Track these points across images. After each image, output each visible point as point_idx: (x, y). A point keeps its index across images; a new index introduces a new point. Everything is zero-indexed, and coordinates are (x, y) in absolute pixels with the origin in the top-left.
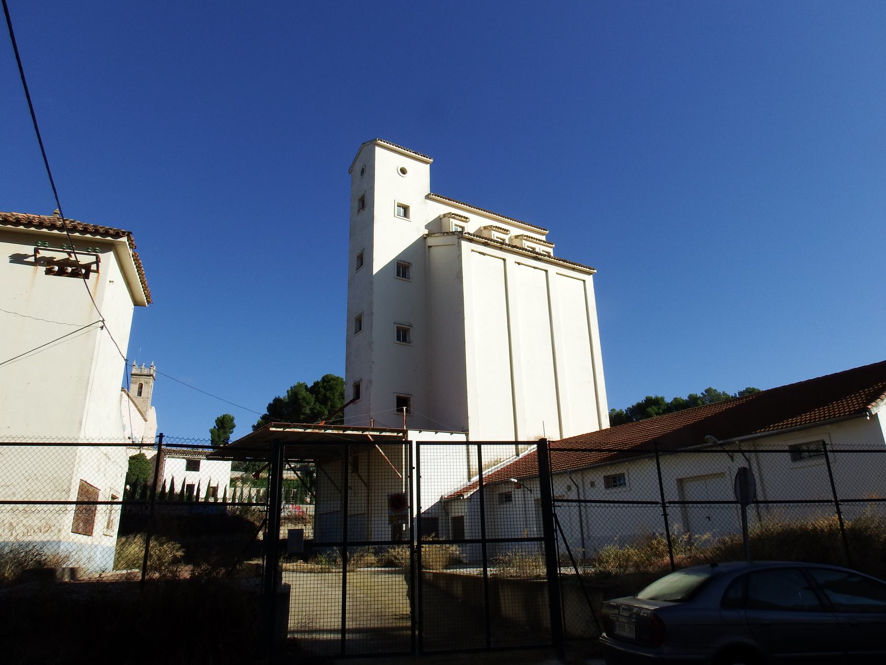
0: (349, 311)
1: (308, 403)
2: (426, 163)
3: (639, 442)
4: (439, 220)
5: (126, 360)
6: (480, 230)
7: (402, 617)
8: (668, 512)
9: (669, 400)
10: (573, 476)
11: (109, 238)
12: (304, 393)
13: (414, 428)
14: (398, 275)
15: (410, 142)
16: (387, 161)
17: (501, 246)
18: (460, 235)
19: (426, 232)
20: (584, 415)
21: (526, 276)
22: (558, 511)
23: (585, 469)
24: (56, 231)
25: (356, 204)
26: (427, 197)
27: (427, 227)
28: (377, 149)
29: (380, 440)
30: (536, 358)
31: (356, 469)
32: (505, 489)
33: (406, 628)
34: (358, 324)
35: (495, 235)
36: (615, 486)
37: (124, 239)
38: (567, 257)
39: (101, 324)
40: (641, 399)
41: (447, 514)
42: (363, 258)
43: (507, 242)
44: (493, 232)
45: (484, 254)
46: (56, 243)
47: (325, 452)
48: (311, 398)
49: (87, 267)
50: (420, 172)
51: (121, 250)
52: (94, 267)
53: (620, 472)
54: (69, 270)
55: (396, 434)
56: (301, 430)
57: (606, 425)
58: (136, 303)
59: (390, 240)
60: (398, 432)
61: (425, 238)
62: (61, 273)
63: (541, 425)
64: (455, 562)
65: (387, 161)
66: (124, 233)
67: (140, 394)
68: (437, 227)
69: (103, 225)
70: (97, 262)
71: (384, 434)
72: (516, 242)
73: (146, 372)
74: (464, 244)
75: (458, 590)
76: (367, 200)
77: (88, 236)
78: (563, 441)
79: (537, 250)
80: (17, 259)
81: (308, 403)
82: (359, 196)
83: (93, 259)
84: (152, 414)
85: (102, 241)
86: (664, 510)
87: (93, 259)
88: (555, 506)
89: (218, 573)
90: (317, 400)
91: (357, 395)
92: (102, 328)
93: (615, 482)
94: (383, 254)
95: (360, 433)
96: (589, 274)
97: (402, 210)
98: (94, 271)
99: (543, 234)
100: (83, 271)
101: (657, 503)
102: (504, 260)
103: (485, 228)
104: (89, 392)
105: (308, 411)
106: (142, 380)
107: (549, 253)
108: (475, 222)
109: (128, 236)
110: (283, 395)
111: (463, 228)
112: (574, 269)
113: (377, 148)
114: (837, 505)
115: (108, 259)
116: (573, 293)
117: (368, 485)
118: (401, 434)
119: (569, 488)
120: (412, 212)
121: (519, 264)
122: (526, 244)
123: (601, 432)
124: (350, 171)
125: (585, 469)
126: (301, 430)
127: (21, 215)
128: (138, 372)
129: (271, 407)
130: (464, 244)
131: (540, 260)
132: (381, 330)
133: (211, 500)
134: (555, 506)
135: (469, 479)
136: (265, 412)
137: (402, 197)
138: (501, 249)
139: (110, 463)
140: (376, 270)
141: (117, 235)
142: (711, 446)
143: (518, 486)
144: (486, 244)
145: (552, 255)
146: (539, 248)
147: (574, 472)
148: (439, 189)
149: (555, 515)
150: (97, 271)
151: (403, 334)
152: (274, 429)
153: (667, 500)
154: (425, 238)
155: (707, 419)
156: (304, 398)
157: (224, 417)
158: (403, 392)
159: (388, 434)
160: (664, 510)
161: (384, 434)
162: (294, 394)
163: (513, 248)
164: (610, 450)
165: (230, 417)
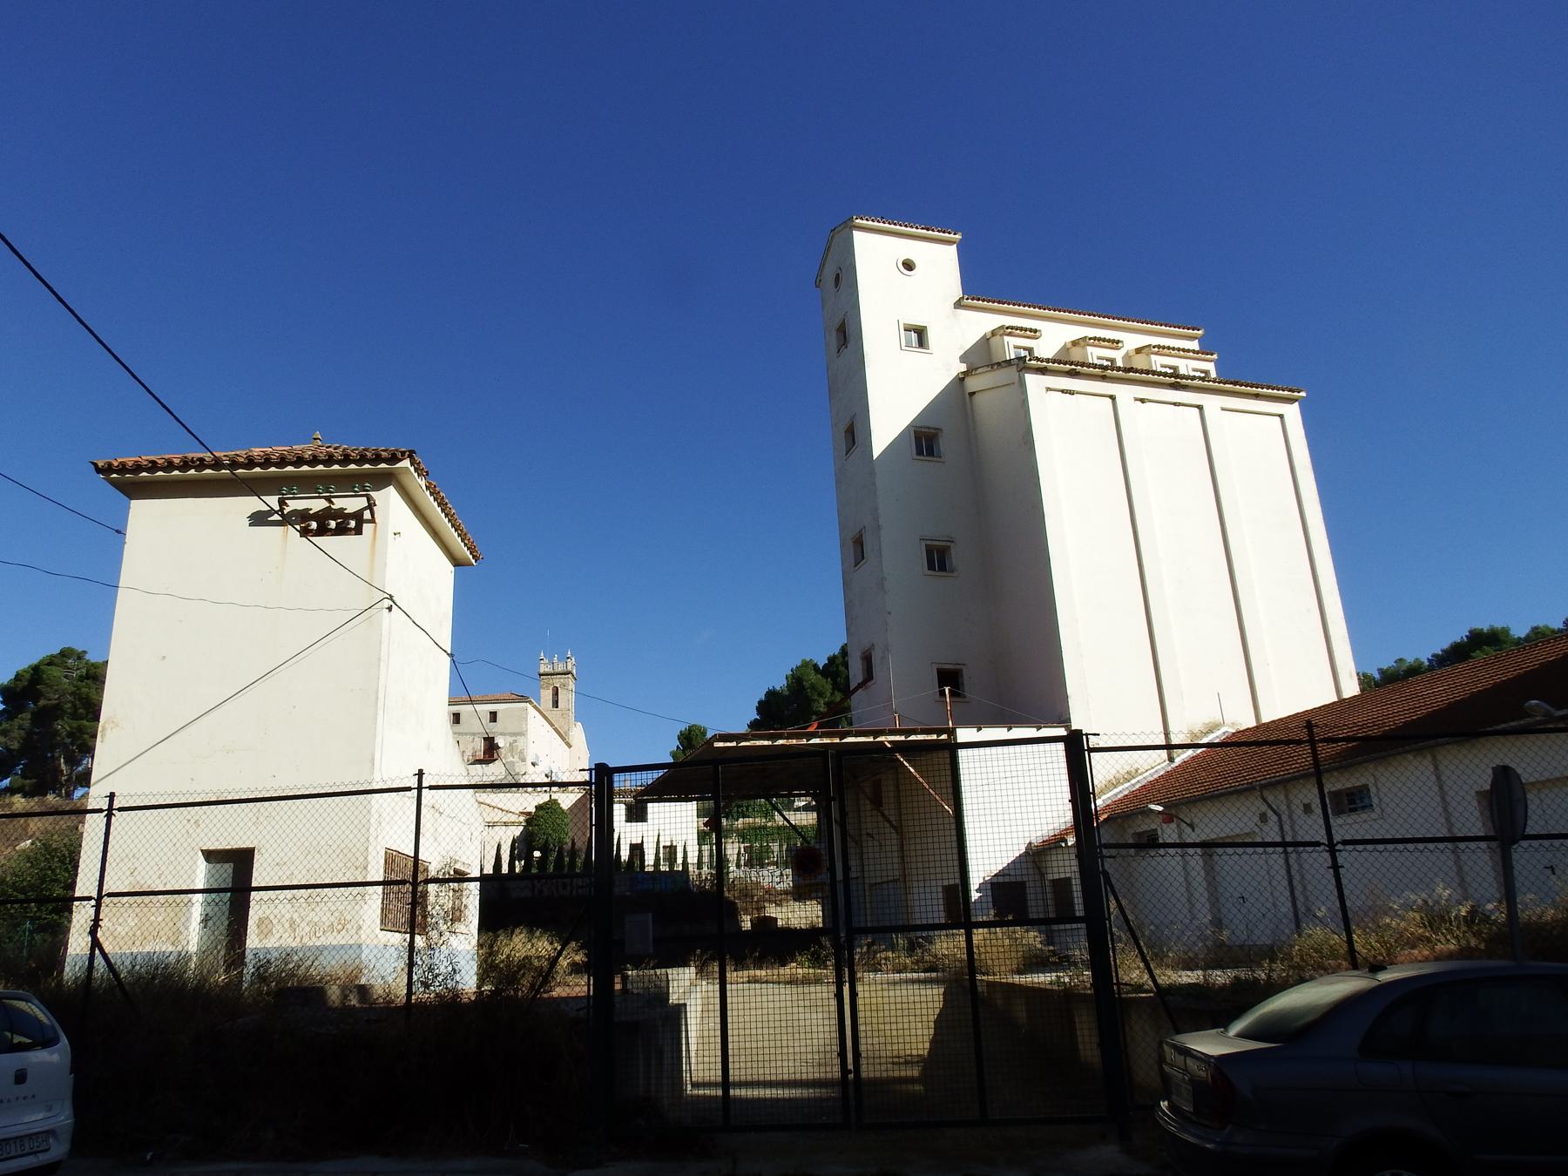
0: (842, 527)
1: (821, 695)
2: (949, 242)
3: (1401, 720)
4: (985, 343)
5: (451, 655)
6: (1065, 349)
7: (908, 1062)
8: (1340, 861)
9: (1520, 631)
10: (1266, 793)
11: (383, 465)
12: (813, 678)
13: (967, 723)
14: (920, 452)
15: (912, 211)
16: (875, 253)
17: (1105, 372)
18: (1022, 365)
19: (963, 367)
20: (1305, 666)
21: (1159, 422)
22: (1109, 865)
23: (1288, 780)
24: (305, 468)
25: (833, 339)
26: (958, 305)
27: (963, 359)
28: (857, 235)
29: (907, 749)
30: (1196, 576)
31: (877, 802)
32: (1145, 826)
33: (911, 1080)
34: (857, 548)
35: (1095, 354)
36: (1352, 810)
37: (406, 463)
38: (1242, 376)
39: (387, 603)
40: (1459, 634)
41: (1042, 875)
42: (854, 431)
43: (1120, 363)
44: (1090, 349)
45: (1071, 393)
46: (308, 485)
47: (835, 778)
48: (826, 685)
49: (358, 516)
50: (940, 261)
51: (405, 480)
52: (367, 515)
53: (1363, 781)
54: (333, 524)
55: (934, 737)
56: (766, 743)
57: (1351, 689)
58: (457, 562)
60: (939, 732)
61: (962, 380)
62: (323, 531)
63: (1213, 704)
64: (1034, 962)
65: (875, 253)
66: (403, 453)
67: (556, 704)
68: (982, 356)
69: (383, 447)
70: (371, 506)
71: (913, 738)
72: (1139, 362)
73: (560, 668)
74: (1030, 379)
75: (1020, 1012)
76: (850, 330)
77: (353, 466)
78: (1261, 727)
79: (1182, 371)
80: (259, 519)
81: (821, 695)
82: (837, 322)
83: (363, 502)
84: (578, 734)
85: (373, 472)
86: (1334, 859)
87: (363, 502)
88: (1103, 857)
89: (516, 990)
90: (836, 686)
91: (869, 675)
92: (390, 609)
93: (1352, 802)
94: (888, 422)
95: (871, 739)
96: (1290, 401)
97: (914, 336)
98: (368, 521)
99: (1192, 338)
100: (353, 524)
101: (1318, 844)
102: (1113, 398)
103: (1075, 343)
104: (380, 712)
105: (823, 709)
106: (557, 681)
107: (1207, 372)
108: (1054, 335)
109: (410, 456)
110: (780, 683)
111: (1030, 350)
112: (1257, 396)
113: (855, 233)
114: (1333, 852)
115: (389, 500)
116: (1267, 442)
117: (899, 829)
118: (944, 737)
119: (1263, 818)
120: (931, 336)
121: (1142, 401)
122: (1158, 362)
123: (1342, 705)
125: (1288, 780)
126: (766, 743)
127: (257, 452)
128: (548, 669)
129: (762, 707)
130: (1030, 379)
132: (898, 555)
133: (664, 868)
134: (1103, 857)
136: (754, 716)
137: (912, 313)
138: (1104, 378)
139: (441, 820)
140: (877, 451)
141: (394, 459)
142: (1539, 723)
143: (1168, 817)
144: (1072, 374)
145: (1213, 375)
146: (1186, 366)
147: (1271, 785)
148: (979, 286)
149: (1106, 874)
150: (373, 521)
151: (938, 558)
152: (721, 744)
153: (1337, 838)
154: (962, 380)
155: (1545, 667)
156: (813, 687)
157: (691, 729)
158: (949, 660)
159: (920, 737)
160: (1334, 859)
161: (913, 738)
162: (797, 680)
163: (1129, 374)
164: (1347, 739)
165: (699, 728)
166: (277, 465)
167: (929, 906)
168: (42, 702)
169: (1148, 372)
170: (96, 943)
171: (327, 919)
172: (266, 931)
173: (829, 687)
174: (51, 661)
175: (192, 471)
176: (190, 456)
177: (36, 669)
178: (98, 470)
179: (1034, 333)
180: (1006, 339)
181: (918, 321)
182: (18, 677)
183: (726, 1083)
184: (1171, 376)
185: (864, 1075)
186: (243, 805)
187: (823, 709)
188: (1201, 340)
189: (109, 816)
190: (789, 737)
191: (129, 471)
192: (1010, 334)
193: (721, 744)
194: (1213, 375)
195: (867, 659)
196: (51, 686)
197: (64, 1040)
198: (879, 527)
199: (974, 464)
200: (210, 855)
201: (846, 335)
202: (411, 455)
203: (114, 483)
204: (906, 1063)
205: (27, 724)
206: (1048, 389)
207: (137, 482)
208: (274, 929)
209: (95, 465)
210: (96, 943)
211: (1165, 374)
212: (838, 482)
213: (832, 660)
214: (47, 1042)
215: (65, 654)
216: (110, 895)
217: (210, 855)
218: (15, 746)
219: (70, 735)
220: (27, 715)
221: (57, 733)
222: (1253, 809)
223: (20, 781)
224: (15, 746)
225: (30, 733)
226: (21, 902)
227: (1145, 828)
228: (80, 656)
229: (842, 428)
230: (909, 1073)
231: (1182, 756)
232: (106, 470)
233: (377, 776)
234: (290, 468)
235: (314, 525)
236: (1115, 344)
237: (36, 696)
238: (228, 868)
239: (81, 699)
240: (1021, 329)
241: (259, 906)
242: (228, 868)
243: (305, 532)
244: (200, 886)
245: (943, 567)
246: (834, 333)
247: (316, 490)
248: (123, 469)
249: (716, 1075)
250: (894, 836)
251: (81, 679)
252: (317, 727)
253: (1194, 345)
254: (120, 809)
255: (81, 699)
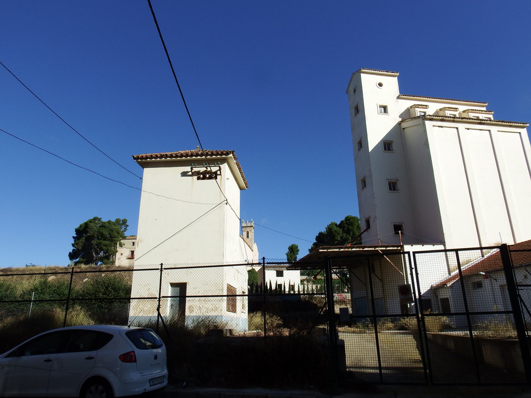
0: (357, 176)
1: (338, 234)
4: (408, 111)
5: (240, 220)
6: (437, 112)
11: (224, 156)
12: (335, 228)
13: (408, 243)
15: (381, 66)
16: (369, 81)
17: (454, 119)
18: (424, 117)
19: (400, 119)
21: (475, 137)
24: (199, 157)
25: (353, 111)
26: (398, 98)
27: (400, 116)
32: (476, 279)
33: (420, 368)
34: (363, 183)
35: (448, 113)
37: (231, 155)
38: (504, 118)
39: (226, 202)
41: (437, 297)
42: (362, 143)
43: (457, 116)
44: (446, 112)
45: (442, 127)
46: (200, 163)
47: (355, 261)
48: (340, 231)
49: (216, 173)
50: (391, 83)
52: (219, 173)
54: (208, 176)
55: (396, 248)
56: (337, 250)
58: (241, 189)
59: (377, 129)
60: (398, 246)
62: (204, 178)
65: (369, 81)
66: (230, 152)
67: (248, 237)
68: (407, 115)
69: (220, 150)
70: (220, 170)
71: (388, 248)
72: (464, 115)
73: (249, 225)
76: (359, 108)
77: (214, 156)
78: (516, 245)
80: (184, 174)
81: (338, 234)
82: (355, 106)
83: (218, 168)
84: (255, 247)
87: (218, 168)
88: (518, 290)
92: (226, 204)
94: (374, 140)
97: (383, 109)
98: (219, 175)
103: (440, 110)
105: (339, 239)
108: (433, 107)
109: (233, 153)
110: (324, 230)
111: (425, 113)
112: (510, 126)
115: (225, 167)
117: (382, 280)
118: (399, 248)
121: (468, 129)
122: (472, 115)
124: (347, 92)
126: (337, 250)
129: (318, 238)
130: (427, 122)
131: (484, 124)
132: (378, 185)
133: (292, 292)
135: (450, 274)
138: (454, 121)
140: (370, 150)
141: (227, 154)
143: (486, 277)
145: (492, 119)
146: (482, 116)
148: (406, 90)
149: (519, 296)
150: (220, 175)
151: (393, 186)
152: (322, 250)
156: (336, 231)
158: (397, 222)
161: (388, 248)
162: (330, 229)
163: (463, 120)
166: (190, 156)
167: (394, 306)
168: (88, 234)
169: (468, 119)
170: (159, 314)
171: (211, 307)
172: (191, 311)
173: (341, 231)
174: (91, 221)
175: (163, 159)
176: (162, 153)
177: (86, 224)
178: (134, 158)
179: (426, 107)
180: (416, 109)
181: (384, 104)
182: (81, 226)
183: (380, 368)
184: (476, 120)
185: (382, 366)
186: (195, 269)
187: (339, 239)
188: (487, 107)
189: (161, 271)
190: (345, 248)
191: (144, 159)
192: (417, 107)
193: (322, 250)
194: (492, 119)
195: (368, 222)
196: (90, 229)
197: (164, 346)
198: (371, 176)
199: (407, 154)
200: (173, 285)
201: (358, 109)
202: (233, 152)
203: (139, 163)
204: (415, 362)
205: (84, 241)
206: (434, 126)
207: (145, 162)
208: (195, 310)
209: (134, 157)
210: (159, 314)
211: (474, 119)
212: (355, 160)
213: (342, 222)
214: (159, 347)
215: (95, 219)
216: (163, 297)
217: (173, 285)
218: (80, 248)
219: (97, 245)
220: (84, 238)
221: (92, 244)
222: (523, 273)
223: (82, 260)
224: (80, 248)
225: (84, 244)
226: (41, 301)
227: (476, 280)
228: (100, 220)
229: (357, 141)
230: (419, 366)
231: (488, 254)
232: (137, 158)
233: (225, 261)
234: (194, 157)
235: (202, 176)
236: (456, 109)
237: (86, 232)
238: (178, 289)
239: (100, 233)
240: (422, 105)
241: (189, 302)
242: (178, 289)
243: (199, 178)
244: (170, 295)
245: (394, 189)
246: (353, 110)
247: (203, 164)
248: (142, 158)
249: (375, 363)
250: (380, 282)
251: (100, 227)
252: (199, 243)
253: (484, 109)
254: (165, 269)
255: (100, 233)
